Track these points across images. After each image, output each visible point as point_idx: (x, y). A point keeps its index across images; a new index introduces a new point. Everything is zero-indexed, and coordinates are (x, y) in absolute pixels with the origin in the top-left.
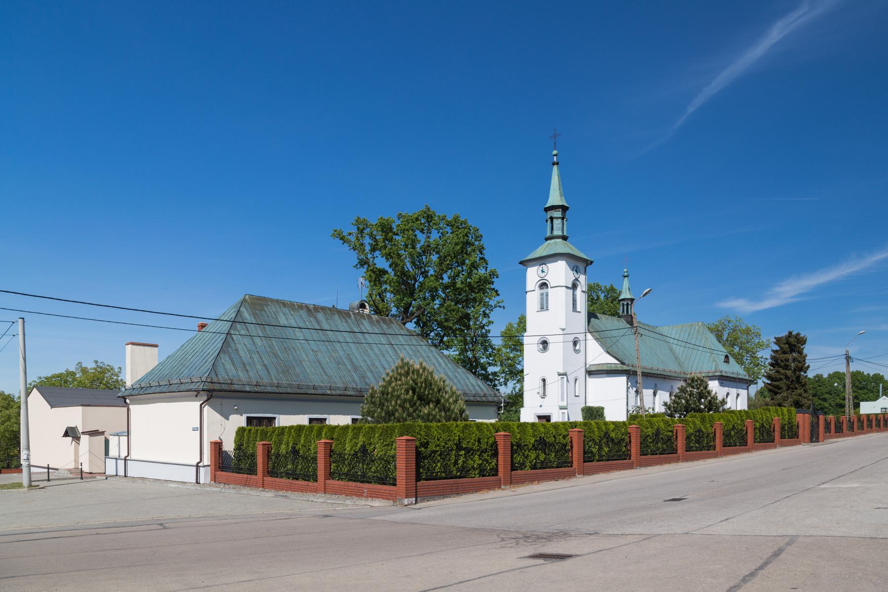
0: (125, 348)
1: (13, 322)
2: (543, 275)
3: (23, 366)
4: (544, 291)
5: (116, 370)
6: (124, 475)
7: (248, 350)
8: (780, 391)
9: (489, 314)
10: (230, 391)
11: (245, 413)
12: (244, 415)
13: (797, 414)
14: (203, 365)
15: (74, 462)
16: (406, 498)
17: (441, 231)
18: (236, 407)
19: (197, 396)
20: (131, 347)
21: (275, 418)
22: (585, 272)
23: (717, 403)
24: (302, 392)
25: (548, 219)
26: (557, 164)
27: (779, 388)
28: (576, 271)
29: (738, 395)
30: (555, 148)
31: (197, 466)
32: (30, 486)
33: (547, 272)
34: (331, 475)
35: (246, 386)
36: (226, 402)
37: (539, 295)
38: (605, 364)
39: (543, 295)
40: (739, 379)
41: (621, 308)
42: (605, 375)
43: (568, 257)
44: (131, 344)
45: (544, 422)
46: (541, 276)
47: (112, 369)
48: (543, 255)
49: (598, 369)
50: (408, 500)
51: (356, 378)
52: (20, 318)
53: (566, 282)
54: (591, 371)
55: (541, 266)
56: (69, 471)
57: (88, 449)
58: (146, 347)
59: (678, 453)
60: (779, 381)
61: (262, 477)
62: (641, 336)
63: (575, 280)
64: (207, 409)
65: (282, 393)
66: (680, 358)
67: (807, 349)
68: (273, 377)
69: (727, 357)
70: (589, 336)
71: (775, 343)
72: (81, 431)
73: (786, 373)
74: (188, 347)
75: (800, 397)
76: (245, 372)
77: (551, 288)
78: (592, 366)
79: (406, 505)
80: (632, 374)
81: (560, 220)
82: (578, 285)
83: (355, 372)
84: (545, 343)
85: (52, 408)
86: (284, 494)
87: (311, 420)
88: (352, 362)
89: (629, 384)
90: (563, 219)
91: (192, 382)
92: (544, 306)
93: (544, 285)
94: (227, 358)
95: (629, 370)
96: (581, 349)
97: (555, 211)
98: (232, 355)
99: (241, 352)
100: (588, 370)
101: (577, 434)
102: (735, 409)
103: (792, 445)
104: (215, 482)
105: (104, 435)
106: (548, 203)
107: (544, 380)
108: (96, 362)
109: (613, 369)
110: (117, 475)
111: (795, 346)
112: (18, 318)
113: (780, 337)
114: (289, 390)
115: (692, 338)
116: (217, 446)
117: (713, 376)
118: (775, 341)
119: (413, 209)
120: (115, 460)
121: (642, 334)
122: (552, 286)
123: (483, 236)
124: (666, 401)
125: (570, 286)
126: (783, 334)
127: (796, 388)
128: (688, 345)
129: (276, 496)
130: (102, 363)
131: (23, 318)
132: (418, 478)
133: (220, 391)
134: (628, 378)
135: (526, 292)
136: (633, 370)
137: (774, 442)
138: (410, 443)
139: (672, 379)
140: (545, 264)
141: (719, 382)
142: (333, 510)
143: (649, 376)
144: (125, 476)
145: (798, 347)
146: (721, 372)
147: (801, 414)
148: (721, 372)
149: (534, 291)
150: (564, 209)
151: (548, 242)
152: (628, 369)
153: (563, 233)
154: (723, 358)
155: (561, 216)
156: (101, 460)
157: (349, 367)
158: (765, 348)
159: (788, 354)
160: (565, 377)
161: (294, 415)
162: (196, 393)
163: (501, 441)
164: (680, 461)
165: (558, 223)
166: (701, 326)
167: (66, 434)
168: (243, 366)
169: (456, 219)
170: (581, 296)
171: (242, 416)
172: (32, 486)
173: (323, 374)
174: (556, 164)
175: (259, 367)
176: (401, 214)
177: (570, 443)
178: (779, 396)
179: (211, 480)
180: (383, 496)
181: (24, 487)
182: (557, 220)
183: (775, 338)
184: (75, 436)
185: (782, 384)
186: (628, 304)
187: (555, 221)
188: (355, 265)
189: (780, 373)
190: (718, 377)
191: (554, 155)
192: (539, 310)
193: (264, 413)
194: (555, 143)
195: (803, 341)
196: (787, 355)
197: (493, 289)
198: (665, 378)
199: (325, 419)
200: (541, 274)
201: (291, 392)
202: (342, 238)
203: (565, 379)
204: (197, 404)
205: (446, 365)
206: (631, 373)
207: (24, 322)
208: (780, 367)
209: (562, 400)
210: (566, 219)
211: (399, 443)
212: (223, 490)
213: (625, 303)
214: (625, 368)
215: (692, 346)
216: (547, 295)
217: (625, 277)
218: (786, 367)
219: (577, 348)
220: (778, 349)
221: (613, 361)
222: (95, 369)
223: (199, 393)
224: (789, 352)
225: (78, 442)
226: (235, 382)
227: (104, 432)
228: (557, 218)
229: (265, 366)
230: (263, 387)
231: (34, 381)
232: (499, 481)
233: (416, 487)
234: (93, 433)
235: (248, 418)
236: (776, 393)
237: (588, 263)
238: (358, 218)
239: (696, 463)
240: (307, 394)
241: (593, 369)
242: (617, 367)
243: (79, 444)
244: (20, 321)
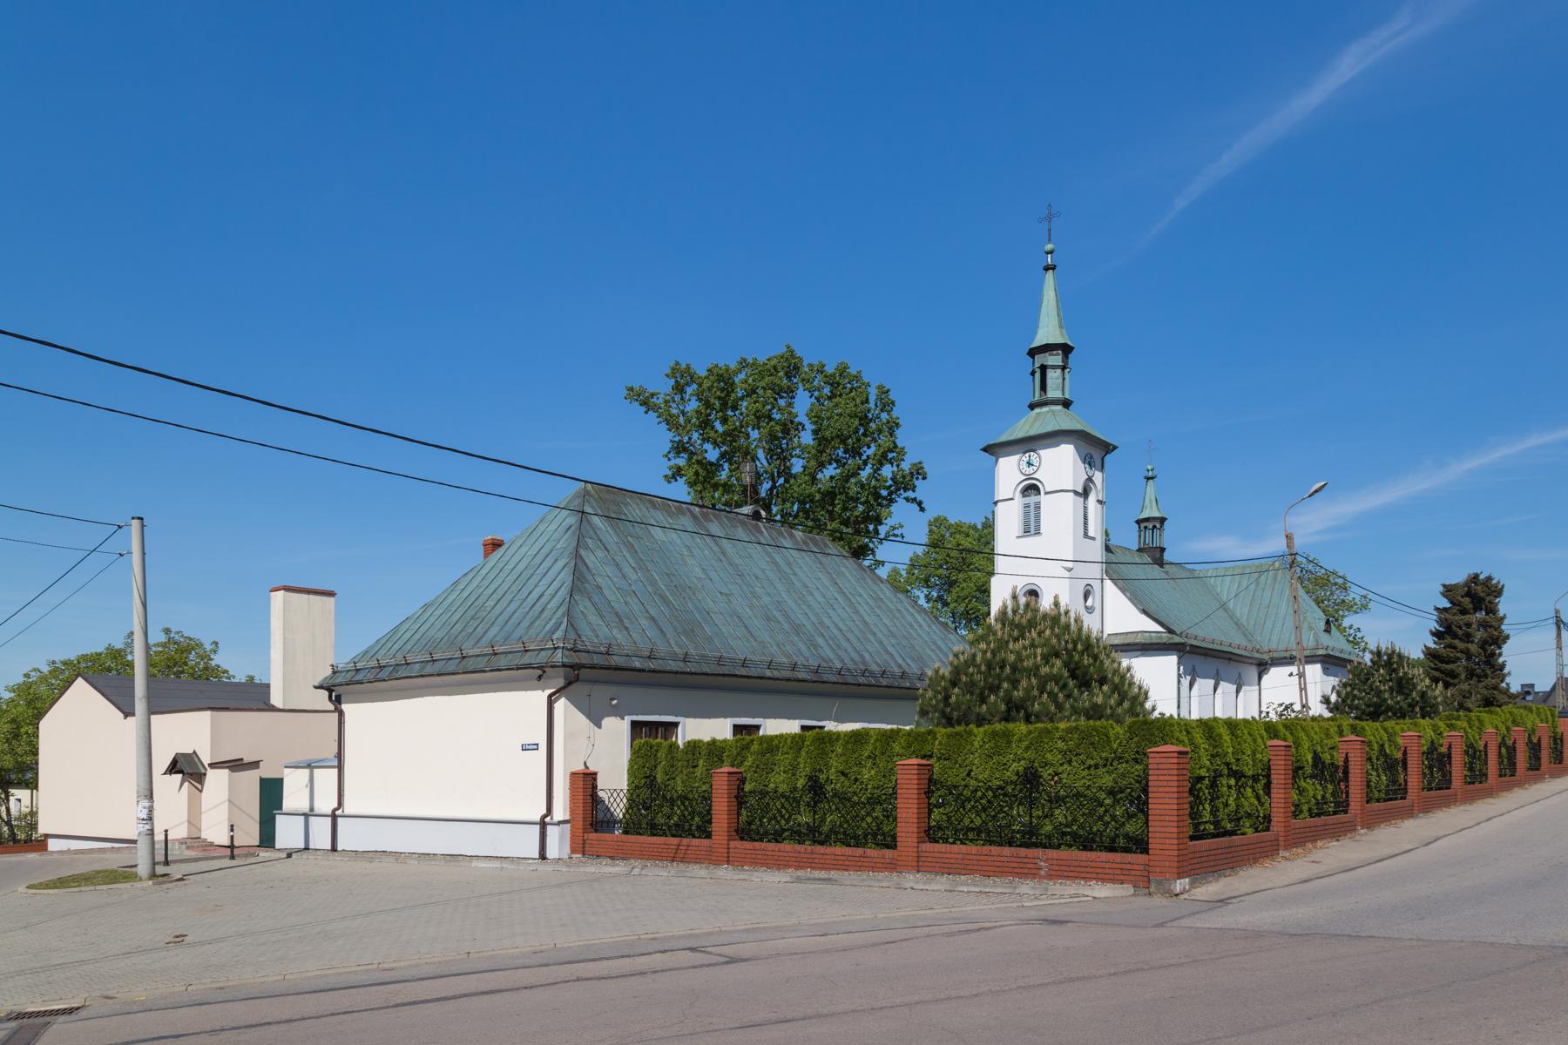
0: (269, 595)
1: (120, 527)
2: (1031, 470)
3: (142, 620)
4: (1032, 499)
5: (208, 647)
6: (329, 847)
7: (617, 589)
8: (1456, 681)
9: (876, 549)
10: (607, 669)
11: (628, 715)
12: (626, 718)
14: (538, 618)
15: (186, 824)
16: (1179, 878)
17: (816, 394)
18: (615, 702)
19: (540, 677)
20: (284, 595)
21: (676, 725)
22: (1103, 467)
23: (1118, 715)
24: (727, 672)
25: (1037, 370)
26: (1053, 268)
27: (1453, 675)
28: (1090, 465)
30: (1050, 240)
31: (543, 825)
32: (153, 875)
33: (1037, 465)
34: (931, 834)
35: (633, 658)
36: (600, 692)
37: (1021, 507)
38: (1138, 632)
39: (1029, 507)
42: (1139, 653)
43: (1079, 437)
44: (284, 589)
46: (1027, 473)
47: (200, 645)
48: (1033, 432)
49: (1126, 642)
50: (1180, 883)
51: (802, 646)
52: (133, 518)
53: (1074, 486)
55: (1027, 455)
56: (182, 843)
57: (226, 797)
58: (312, 596)
60: (1453, 662)
61: (726, 842)
63: (1087, 479)
64: (561, 705)
65: (695, 674)
67: (1504, 606)
68: (672, 642)
70: (1108, 584)
71: (1443, 594)
72: (206, 760)
74: (475, 584)
75: (1495, 692)
76: (625, 632)
77: (1046, 493)
78: (1113, 637)
79: (1177, 895)
80: (1188, 652)
81: (1059, 371)
83: (798, 634)
86: (826, 876)
87: (804, 728)
88: (787, 616)
89: (1182, 668)
90: (1064, 368)
91: (526, 651)
92: (1031, 526)
93: (1031, 489)
94: (588, 604)
96: (1095, 605)
97: (1050, 355)
98: (594, 596)
99: (606, 592)
101: (916, 772)
102: (1234, 717)
104: (584, 854)
105: (258, 768)
106: (1035, 342)
108: (167, 631)
110: (307, 848)
111: (1482, 599)
112: (130, 517)
113: (1453, 583)
114: (706, 669)
115: (1264, 589)
116: (586, 782)
117: (1312, 656)
118: (1442, 589)
119: (765, 351)
120: (303, 817)
122: (1047, 490)
124: (1326, 693)
125: (1080, 490)
126: (1458, 577)
127: (1486, 676)
129: (799, 879)
130: (178, 633)
131: (141, 519)
133: (593, 667)
134: (1179, 658)
135: (996, 503)
137: (1538, 769)
139: (1241, 662)
140: (1034, 451)
141: (1322, 666)
142: (1018, 907)
143: (1210, 656)
144: (334, 849)
145: (1489, 602)
149: (1012, 499)
150: (1066, 349)
151: (1037, 410)
152: (1182, 641)
153: (1063, 395)
156: (251, 817)
157: (786, 626)
158: (1358, 610)
161: (709, 718)
162: (540, 672)
163: (1279, 758)
164: (1458, 804)
167: (173, 768)
168: (617, 620)
170: (1096, 510)
171: (623, 719)
172: (158, 876)
173: (751, 639)
174: (1051, 268)
175: (644, 622)
176: (745, 361)
179: (573, 851)
180: (1100, 876)
181: (141, 879)
182: (1053, 371)
183: (1444, 586)
184: (195, 771)
186: (1154, 527)
187: (1051, 374)
188: (665, 453)
189: (1455, 648)
191: (1048, 253)
192: (1021, 534)
193: (660, 715)
194: (1050, 230)
195: (1498, 592)
197: (914, 500)
198: (1230, 659)
199: (757, 727)
201: (709, 671)
202: (644, 403)
204: (539, 697)
205: (930, 627)
206: (1188, 648)
207: (143, 526)
208: (1455, 636)
210: (1068, 370)
211: (1158, 760)
212: (636, 871)
214: (1177, 639)
216: (1038, 507)
218: (1468, 638)
219: (1089, 603)
220: (1448, 605)
222: (164, 645)
223: (544, 672)
224: (1472, 611)
225: (199, 786)
226: (615, 650)
227: (259, 762)
228: (1054, 367)
229: (653, 619)
230: (661, 662)
231: (34, 670)
232: (1275, 843)
234: (236, 765)
235: (634, 724)
237: (1108, 448)
238: (677, 363)
240: (736, 676)
242: (1160, 637)
243: (201, 791)
244: (135, 523)
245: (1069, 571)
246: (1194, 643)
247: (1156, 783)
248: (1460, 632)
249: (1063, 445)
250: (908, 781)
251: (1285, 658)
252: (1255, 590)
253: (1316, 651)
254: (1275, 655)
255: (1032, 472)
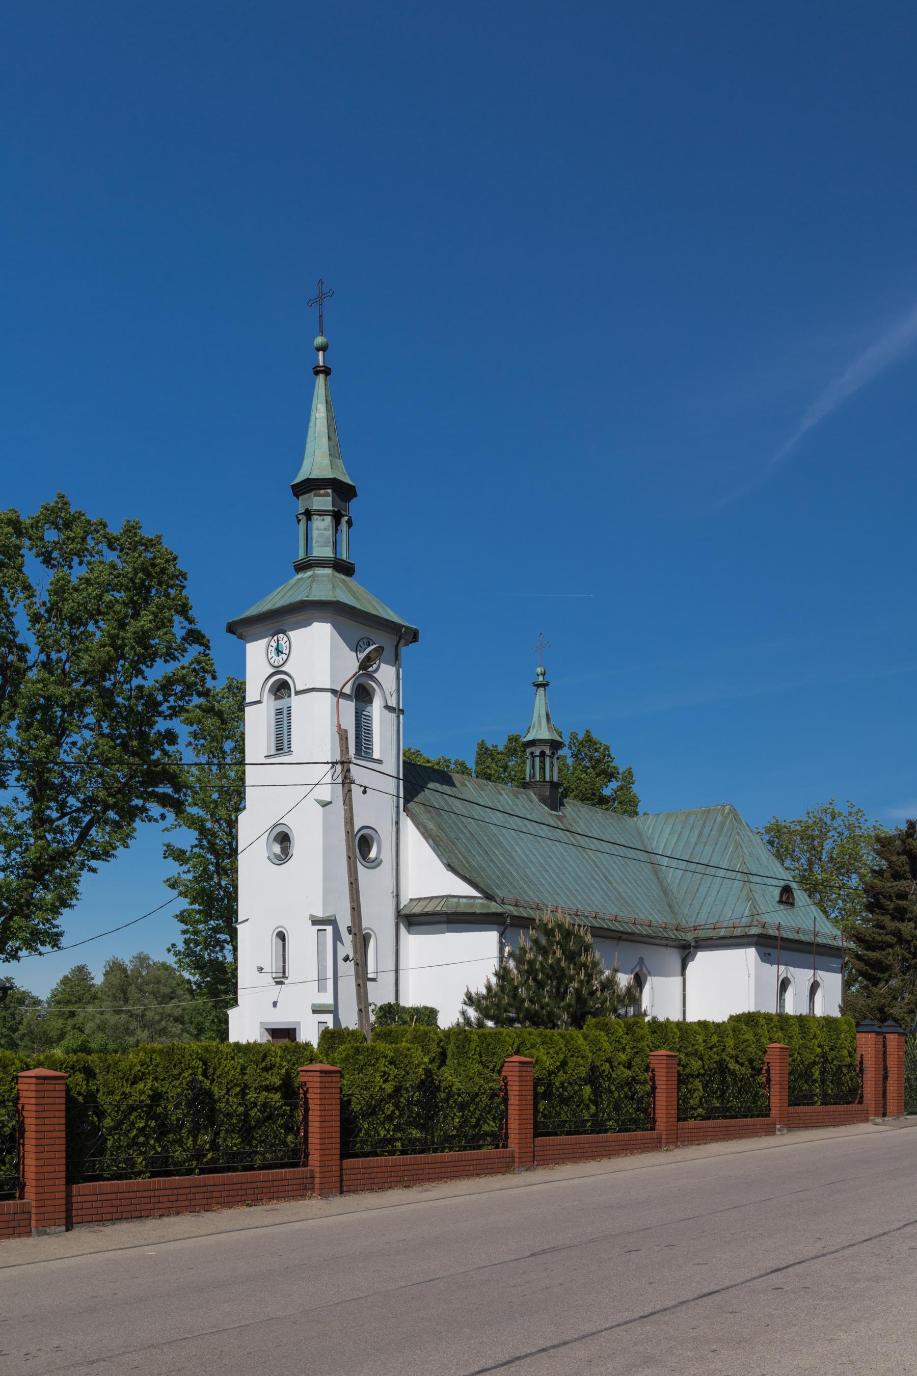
2: (278, 660)
13: (858, 1035)
25: (300, 517)
26: (327, 371)
27: (884, 968)
29: (814, 987)
30: (321, 331)
33: (287, 652)
39: (281, 713)
40: (819, 945)
41: (528, 762)
42: (445, 926)
45: (285, 1042)
53: (333, 682)
54: (414, 915)
55: (275, 638)
59: (310, 1163)
62: (365, 792)
66: (675, 890)
69: (786, 891)
70: (410, 830)
73: (900, 931)
78: (415, 903)
82: (374, 690)
84: (284, 839)
85: (668, 1019)
95: (501, 914)
97: (316, 495)
100: (403, 912)
101: (318, 1079)
103: (835, 1124)
107: (282, 936)
109: (460, 910)
121: (365, 787)
122: (299, 688)
123: (188, 576)
128: (693, 867)
132: (346, 1153)
134: (502, 935)
136: (515, 913)
138: (525, 1069)
140: (284, 632)
146: (763, 927)
147: (869, 1035)
148: (763, 927)
149: (259, 702)
152: (499, 909)
154: (777, 892)
155: (331, 508)
159: (906, 879)
160: (329, 929)
165: (322, 526)
166: (728, 814)
169: (131, 529)
177: (650, 1080)
178: (882, 989)
185: (890, 957)
186: (543, 754)
189: (883, 928)
190: (755, 939)
191: (318, 349)
192: (273, 752)
194: (321, 316)
196: (903, 882)
198: (619, 939)
200: (275, 657)
203: (329, 929)
209: (321, 989)
213: (538, 753)
214: (494, 907)
215: (700, 868)
217: (539, 686)
221: (465, 889)
224: (909, 875)
228: (322, 513)
233: (341, 1170)
236: (875, 981)
239: (151, 1228)
241: (417, 910)
242: (472, 905)
245: (323, 806)
246: (515, 911)
247: (56, 1148)
248: (891, 906)
249: (315, 624)
250: (658, 1062)
251: (711, 939)
252: (696, 844)
253: (747, 929)
254: (701, 934)
255: (281, 662)
